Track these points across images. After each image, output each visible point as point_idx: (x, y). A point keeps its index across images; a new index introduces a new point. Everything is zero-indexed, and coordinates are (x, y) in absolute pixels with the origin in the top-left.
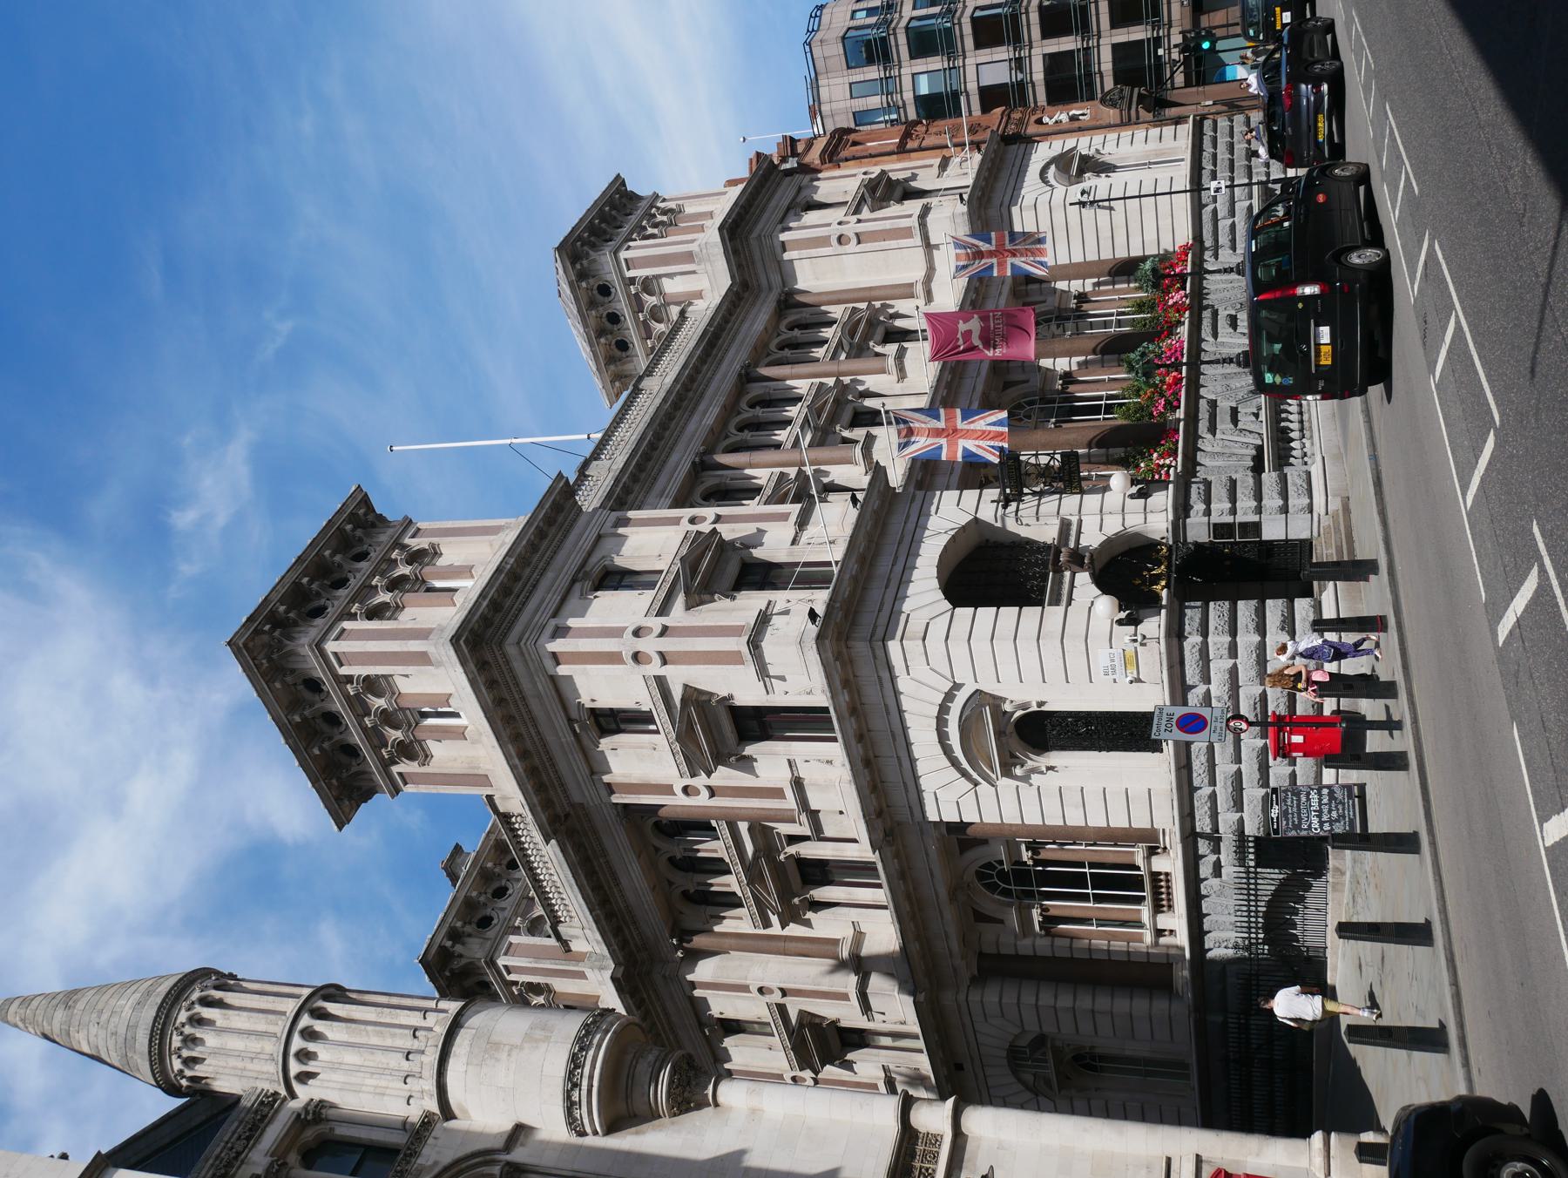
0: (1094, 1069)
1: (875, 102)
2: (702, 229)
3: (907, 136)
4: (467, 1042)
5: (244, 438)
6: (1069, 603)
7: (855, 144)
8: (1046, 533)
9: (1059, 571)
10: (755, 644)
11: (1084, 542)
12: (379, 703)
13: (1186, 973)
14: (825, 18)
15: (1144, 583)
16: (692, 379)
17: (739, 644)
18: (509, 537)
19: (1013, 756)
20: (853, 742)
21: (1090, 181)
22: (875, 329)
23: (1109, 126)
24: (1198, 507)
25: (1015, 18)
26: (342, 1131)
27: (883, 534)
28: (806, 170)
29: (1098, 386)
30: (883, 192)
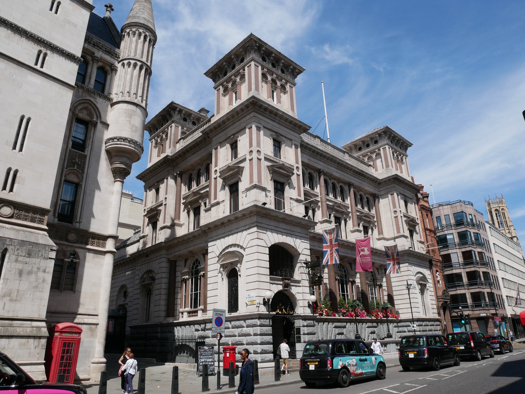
0: (148, 295)
1: (444, 222)
2: (397, 170)
3: (430, 231)
4: (131, 108)
5: (350, 61)
6: (271, 283)
7: (427, 215)
8: (297, 276)
9: (282, 280)
10: (255, 187)
11: (293, 288)
12: (238, 79)
13: (171, 321)
14: (469, 206)
15: (280, 307)
16: (348, 168)
17: (255, 182)
18: (290, 113)
19: (226, 267)
20: (228, 219)
21: (418, 287)
22: (367, 224)
23: (436, 293)
24: (305, 323)
25: (472, 263)
26: (109, 77)
27: (294, 225)
28: (418, 200)
29: (351, 292)
30: (412, 224)
